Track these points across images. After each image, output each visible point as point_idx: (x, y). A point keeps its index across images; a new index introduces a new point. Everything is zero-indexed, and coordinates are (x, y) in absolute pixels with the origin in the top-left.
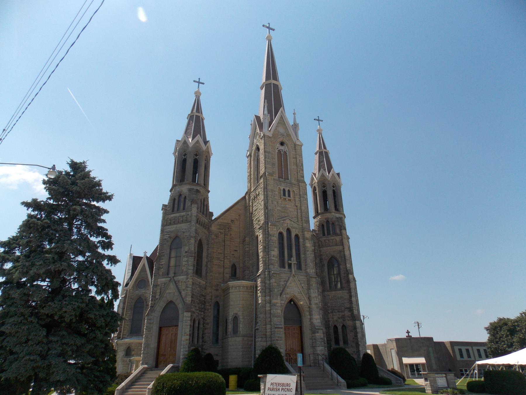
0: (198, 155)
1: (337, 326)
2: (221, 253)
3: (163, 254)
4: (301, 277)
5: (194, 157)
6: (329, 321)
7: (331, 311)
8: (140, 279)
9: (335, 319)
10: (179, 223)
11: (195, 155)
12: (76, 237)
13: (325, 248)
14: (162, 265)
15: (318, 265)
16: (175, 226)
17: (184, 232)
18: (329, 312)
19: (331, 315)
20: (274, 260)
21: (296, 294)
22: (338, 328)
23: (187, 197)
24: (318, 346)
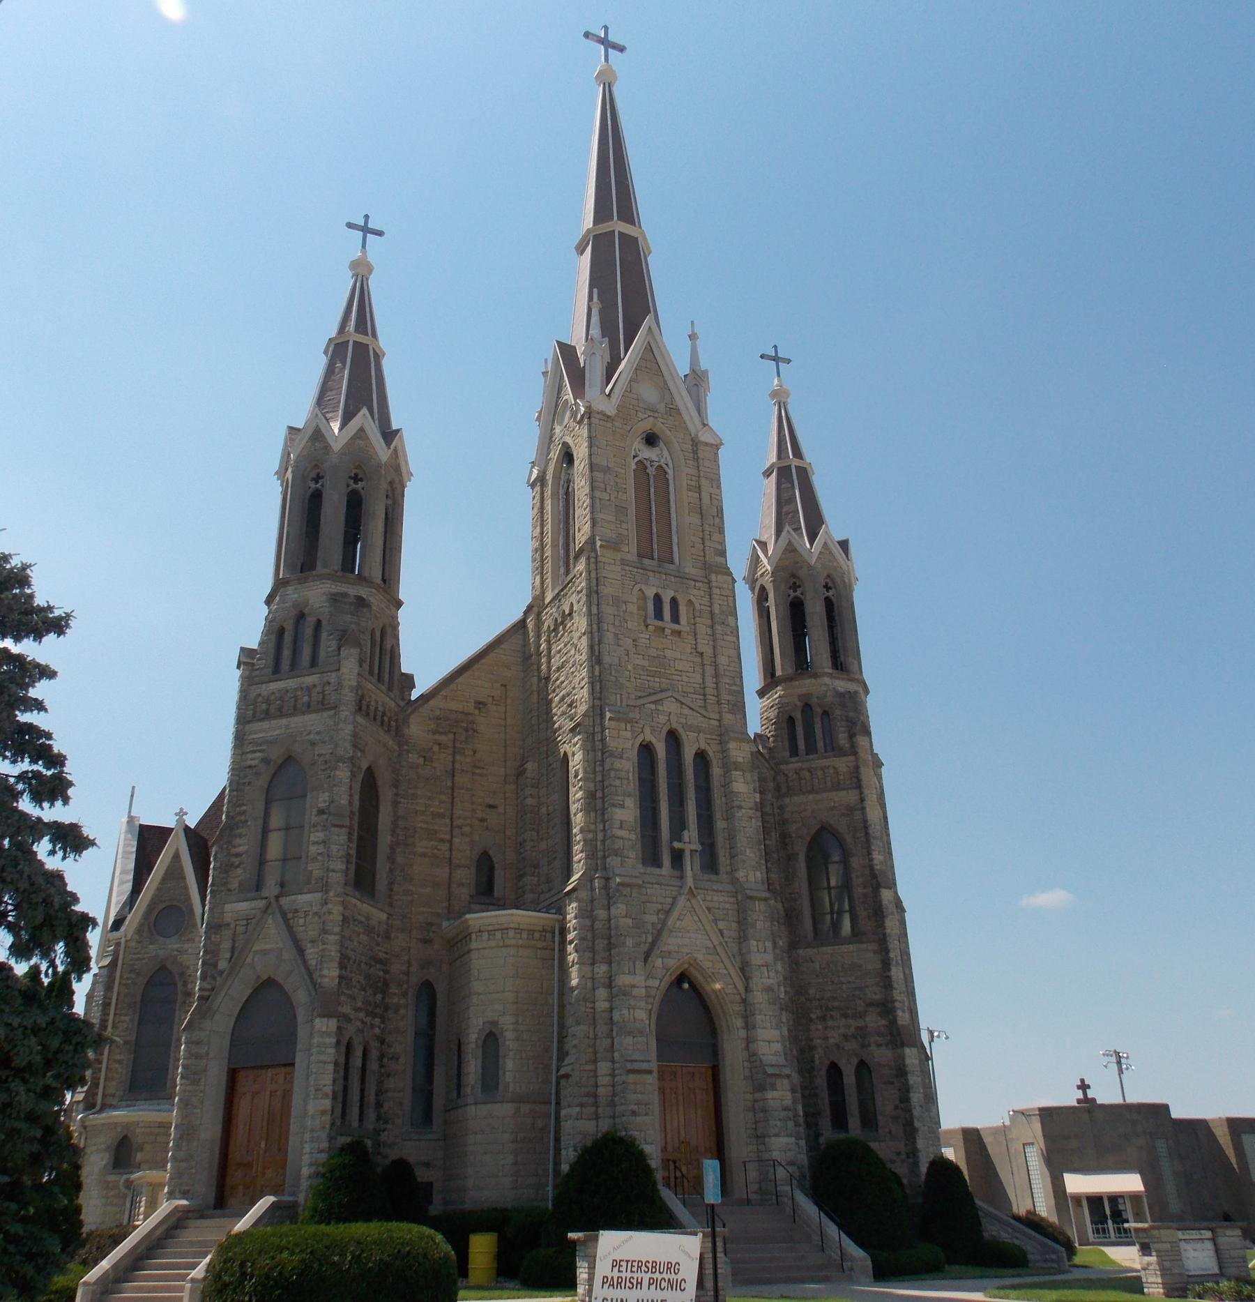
0: (361, 480)
2: (442, 816)
3: (243, 818)
5: (348, 486)
7: (818, 1013)
8: (163, 905)
9: (832, 1040)
10: (295, 711)
11: (350, 477)
14: (238, 855)
15: (775, 856)
16: (284, 721)
17: (313, 744)
18: (813, 1016)
19: (820, 1027)
21: (700, 957)
22: (844, 1073)
23: (324, 623)
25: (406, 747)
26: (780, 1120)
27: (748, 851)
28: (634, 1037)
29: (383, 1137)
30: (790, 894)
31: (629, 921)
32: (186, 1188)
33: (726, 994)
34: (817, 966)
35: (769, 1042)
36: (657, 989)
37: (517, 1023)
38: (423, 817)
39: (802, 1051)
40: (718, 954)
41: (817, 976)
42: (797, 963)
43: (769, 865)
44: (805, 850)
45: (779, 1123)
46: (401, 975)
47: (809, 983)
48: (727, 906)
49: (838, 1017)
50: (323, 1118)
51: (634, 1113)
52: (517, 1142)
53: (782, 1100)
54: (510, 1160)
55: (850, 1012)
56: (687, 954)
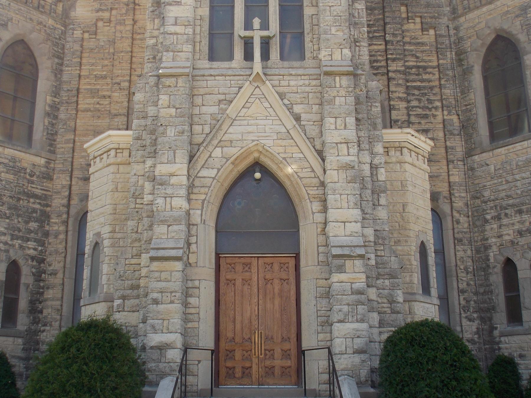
1: (515, 260)
2: (104, 77)
4: (292, 83)
6: (487, 248)
7: (493, 213)
9: (507, 238)
12: (256, 210)
13: (470, 16)
15: (450, 73)
18: (488, 217)
19: (495, 226)
20: (177, 34)
21: (268, 143)
22: (519, 267)
24: (340, 321)
25: (72, 26)
26: (348, 305)
27: (333, 30)
28: (169, 226)
30: (466, 105)
31: (173, 111)
33: (301, 178)
34: (492, 168)
35: (344, 222)
36: (214, 178)
37: (113, 232)
38: (87, 80)
39: (478, 251)
40: (292, 138)
41: (492, 178)
42: (472, 169)
43: (443, 82)
44: (480, 62)
45: (345, 308)
46: (61, 208)
47: (485, 186)
48: (308, 89)
49: (513, 214)
51: (156, 302)
53: (352, 283)
55: (524, 208)
56: (253, 141)
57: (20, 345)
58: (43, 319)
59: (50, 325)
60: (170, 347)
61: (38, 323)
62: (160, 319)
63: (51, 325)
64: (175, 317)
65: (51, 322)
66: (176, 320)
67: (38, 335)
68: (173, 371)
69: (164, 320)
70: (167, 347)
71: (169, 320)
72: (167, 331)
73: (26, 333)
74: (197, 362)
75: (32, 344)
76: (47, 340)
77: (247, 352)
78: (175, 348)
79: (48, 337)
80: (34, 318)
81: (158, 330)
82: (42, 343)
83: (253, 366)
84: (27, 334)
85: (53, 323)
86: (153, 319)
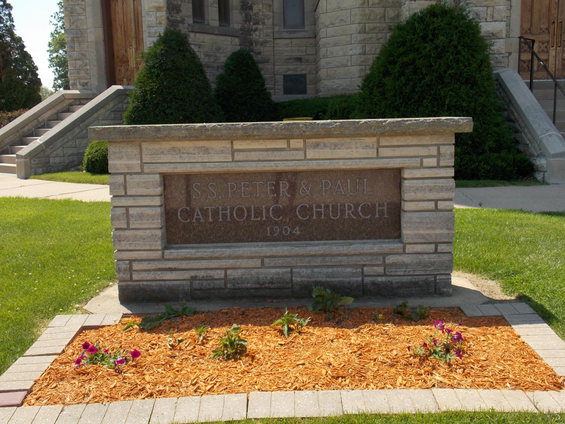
29: (255, 36)
32: (86, 81)
50: (158, 14)
52: (365, 33)
54: (357, 50)
57: (236, 45)
58: (254, 17)
59: (262, 23)
60: (495, 38)
61: (249, 21)
62: (484, 6)
63: (263, 23)
64: (501, 4)
65: (264, 19)
66: (502, 7)
67: (251, 35)
68: (499, 62)
69: (488, 7)
70: (492, 37)
71: (493, 6)
72: (491, 20)
73: (241, 32)
74: (507, 55)
75: (247, 44)
76: (261, 40)
77: (543, 44)
78: (500, 38)
79: (262, 36)
80: (247, 15)
81: (483, 18)
82: (256, 43)
83: (550, 60)
84: (242, 34)
85: (266, 21)
86: (477, 6)
